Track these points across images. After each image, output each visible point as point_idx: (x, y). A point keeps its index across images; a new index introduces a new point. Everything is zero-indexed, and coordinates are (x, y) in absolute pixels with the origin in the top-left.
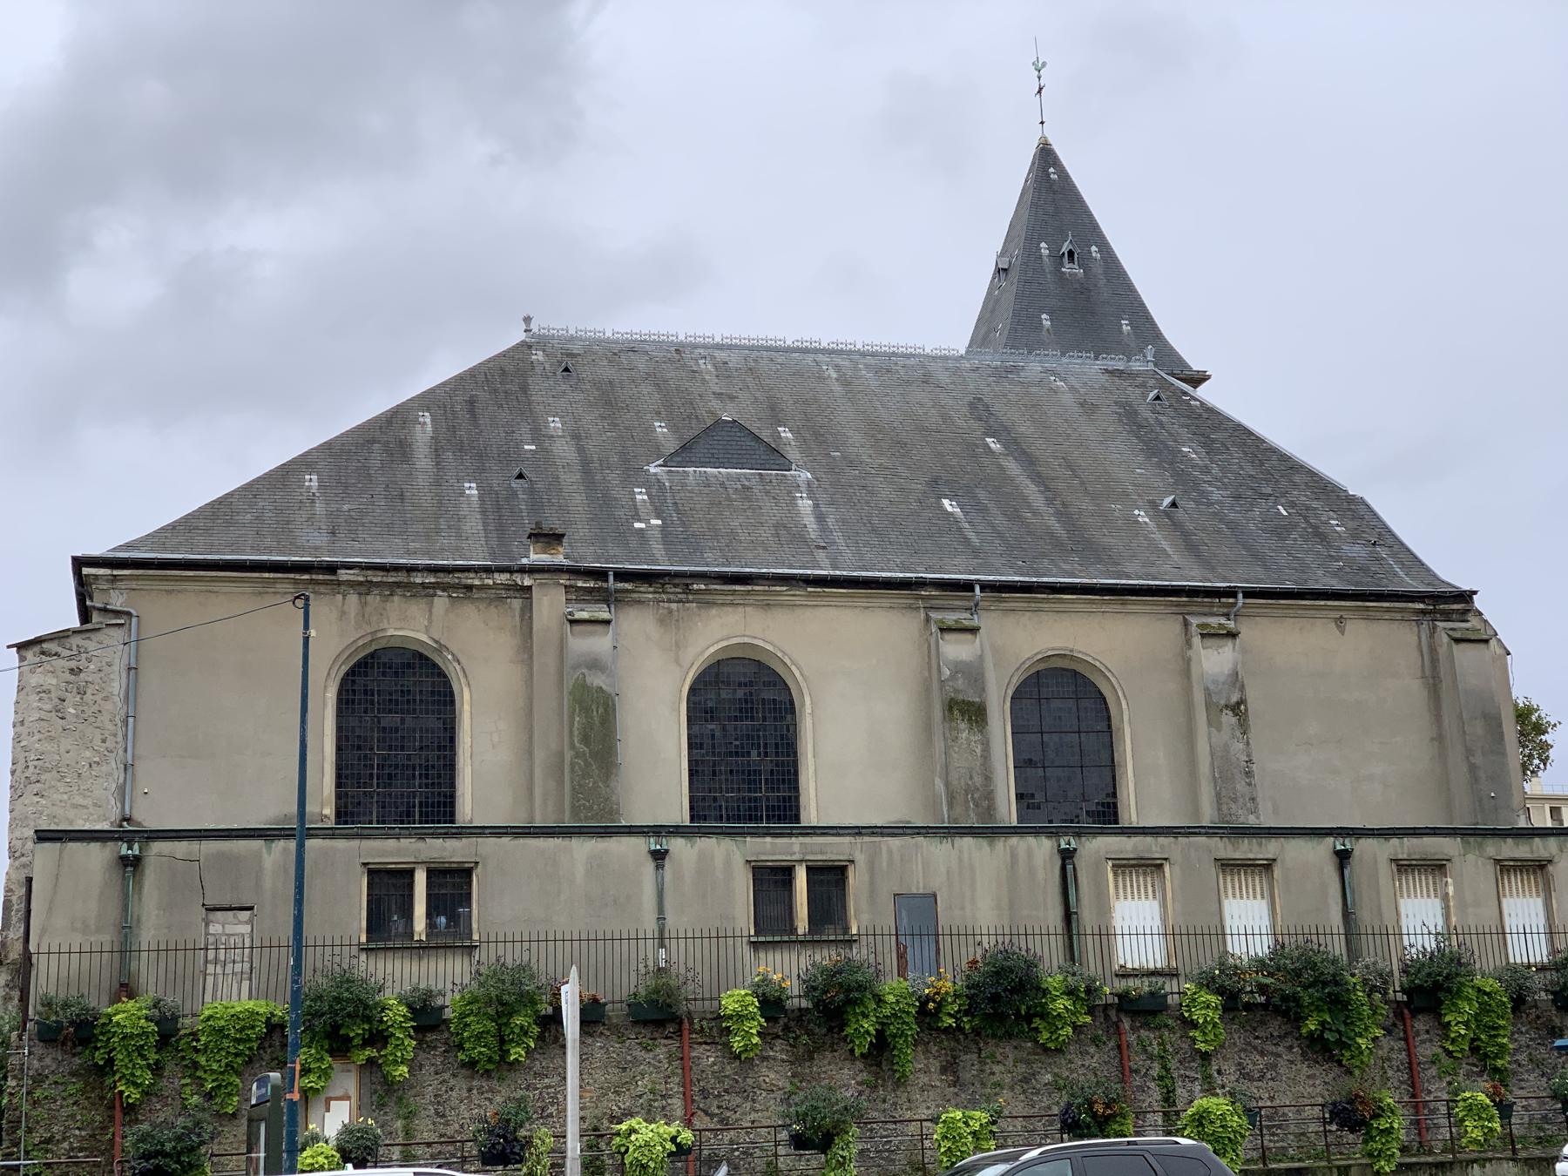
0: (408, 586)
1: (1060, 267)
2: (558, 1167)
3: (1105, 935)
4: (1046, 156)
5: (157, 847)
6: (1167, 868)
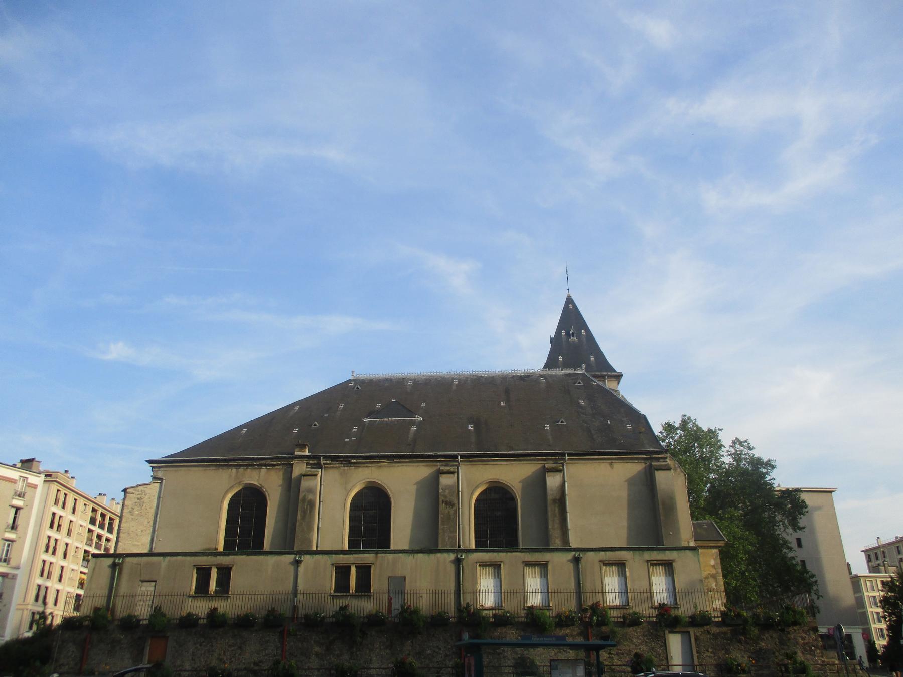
0: (253, 466)
1: (573, 339)
2: (470, 676)
3: (475, 593)
4: (569, 301)
5: (128, 559)
6: (502, 566)
